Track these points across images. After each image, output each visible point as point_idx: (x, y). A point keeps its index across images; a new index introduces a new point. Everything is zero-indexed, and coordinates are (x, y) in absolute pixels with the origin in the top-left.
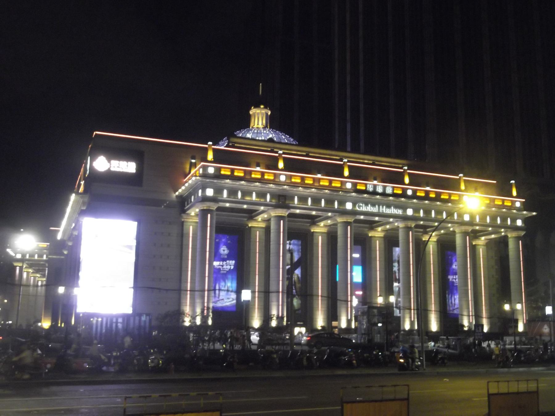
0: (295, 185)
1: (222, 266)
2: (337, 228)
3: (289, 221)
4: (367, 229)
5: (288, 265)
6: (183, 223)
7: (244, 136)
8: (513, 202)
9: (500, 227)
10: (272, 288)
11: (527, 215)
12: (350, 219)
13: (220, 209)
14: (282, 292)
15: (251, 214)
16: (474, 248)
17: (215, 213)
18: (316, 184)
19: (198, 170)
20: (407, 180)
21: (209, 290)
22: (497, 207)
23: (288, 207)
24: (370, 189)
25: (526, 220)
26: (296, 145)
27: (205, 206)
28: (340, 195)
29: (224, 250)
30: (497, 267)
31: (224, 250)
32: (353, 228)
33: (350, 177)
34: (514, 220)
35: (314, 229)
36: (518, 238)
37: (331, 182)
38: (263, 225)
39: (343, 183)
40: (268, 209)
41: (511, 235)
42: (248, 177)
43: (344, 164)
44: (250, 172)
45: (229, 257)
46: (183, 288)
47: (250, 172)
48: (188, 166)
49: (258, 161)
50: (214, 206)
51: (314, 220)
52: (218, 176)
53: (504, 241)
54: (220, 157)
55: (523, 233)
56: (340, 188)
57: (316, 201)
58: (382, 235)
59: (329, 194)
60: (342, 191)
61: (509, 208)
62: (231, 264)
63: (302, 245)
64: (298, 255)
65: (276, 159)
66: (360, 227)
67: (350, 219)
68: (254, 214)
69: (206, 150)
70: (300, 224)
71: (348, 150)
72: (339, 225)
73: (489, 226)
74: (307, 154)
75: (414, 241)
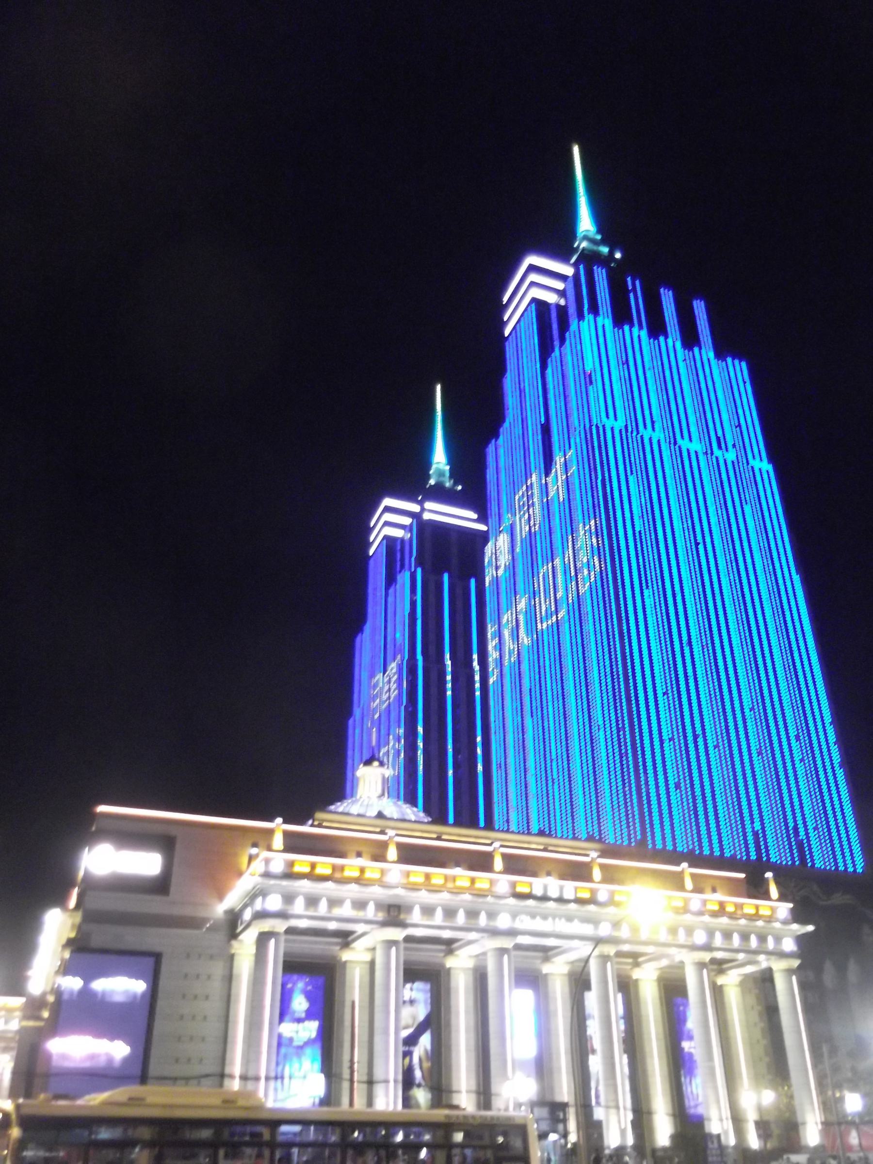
0: (414, 888)
1: (297, 1032)
2: (485, 960)
3: (406, 949)
4: (338, 948)
5: (406, 1027)
6: (232, 957)
7: (346, 811)
8: (773, 910)
9: (756, 952)
10: (378, 1074)
11: (799, 930)
12: (507, 943)
13: (290, 931)
14: (395, 1081)
15: (345, 938)
16: (718, 992)
17: (402, 946)
18: (450, 885)
19: (258, 866)
20: (597, 874)
21: (267, 1079)
22: (748, 917)
23: (403, 925)
24: (538, 892)
25: (801, 940)
26: (429, 823)
27: (266, 925)
28: (488, 903)
29: (300, 1003)
30: (762, 1025)
31: (300, 1004)
32: (513, 959)
33: (780, 900)
34: (778, 940)
35: (546, 969)
36: (790, 972)
37: (473, 881)
38: (368, 957)
39: (492, 882)
40: (372, 929)
41: (779, 966)
42: (338, 875)
43: (494, 850)
44: (342, 868)
45: (310, 1015)
46: (227, 1071)
47: (342, 868)
48: (245, 860)
49: (360, 849)
50: (280, 926)
51: (449, 946)
52: (289, 875)
53: (766, 979)
54: (294, 844)
55: (796, 963)
56: (489, 890)
57: (745, 937)
58: (565, 969)
59: (471, 902)
60: (492, 896)
61: (768, 919)
62: (311, 1028)
63: (432, 991)
64: (426, 1008)
65: (384, 845)
66: (527, 957)
67: (507, 943)
68: (350, 938)
69: (270, 832)
70: (427, 955)
71: (497, 827)
72: (490, 954)
73: (737, 951)
74: (319, 824)
75: (616, 980)
